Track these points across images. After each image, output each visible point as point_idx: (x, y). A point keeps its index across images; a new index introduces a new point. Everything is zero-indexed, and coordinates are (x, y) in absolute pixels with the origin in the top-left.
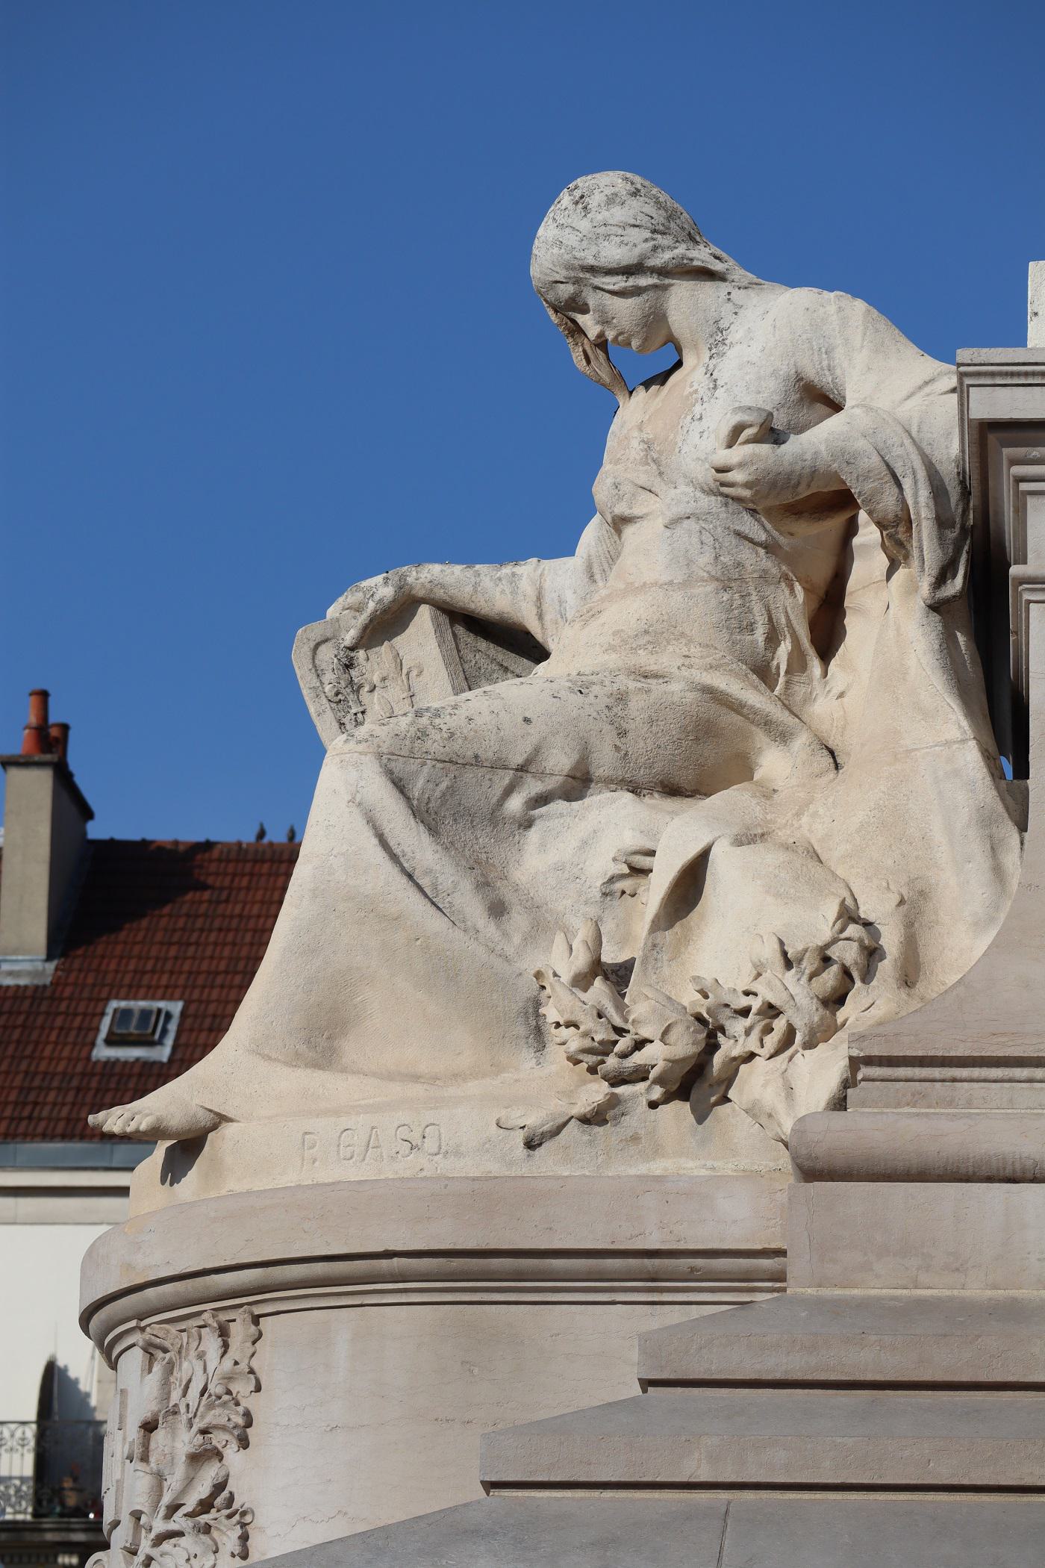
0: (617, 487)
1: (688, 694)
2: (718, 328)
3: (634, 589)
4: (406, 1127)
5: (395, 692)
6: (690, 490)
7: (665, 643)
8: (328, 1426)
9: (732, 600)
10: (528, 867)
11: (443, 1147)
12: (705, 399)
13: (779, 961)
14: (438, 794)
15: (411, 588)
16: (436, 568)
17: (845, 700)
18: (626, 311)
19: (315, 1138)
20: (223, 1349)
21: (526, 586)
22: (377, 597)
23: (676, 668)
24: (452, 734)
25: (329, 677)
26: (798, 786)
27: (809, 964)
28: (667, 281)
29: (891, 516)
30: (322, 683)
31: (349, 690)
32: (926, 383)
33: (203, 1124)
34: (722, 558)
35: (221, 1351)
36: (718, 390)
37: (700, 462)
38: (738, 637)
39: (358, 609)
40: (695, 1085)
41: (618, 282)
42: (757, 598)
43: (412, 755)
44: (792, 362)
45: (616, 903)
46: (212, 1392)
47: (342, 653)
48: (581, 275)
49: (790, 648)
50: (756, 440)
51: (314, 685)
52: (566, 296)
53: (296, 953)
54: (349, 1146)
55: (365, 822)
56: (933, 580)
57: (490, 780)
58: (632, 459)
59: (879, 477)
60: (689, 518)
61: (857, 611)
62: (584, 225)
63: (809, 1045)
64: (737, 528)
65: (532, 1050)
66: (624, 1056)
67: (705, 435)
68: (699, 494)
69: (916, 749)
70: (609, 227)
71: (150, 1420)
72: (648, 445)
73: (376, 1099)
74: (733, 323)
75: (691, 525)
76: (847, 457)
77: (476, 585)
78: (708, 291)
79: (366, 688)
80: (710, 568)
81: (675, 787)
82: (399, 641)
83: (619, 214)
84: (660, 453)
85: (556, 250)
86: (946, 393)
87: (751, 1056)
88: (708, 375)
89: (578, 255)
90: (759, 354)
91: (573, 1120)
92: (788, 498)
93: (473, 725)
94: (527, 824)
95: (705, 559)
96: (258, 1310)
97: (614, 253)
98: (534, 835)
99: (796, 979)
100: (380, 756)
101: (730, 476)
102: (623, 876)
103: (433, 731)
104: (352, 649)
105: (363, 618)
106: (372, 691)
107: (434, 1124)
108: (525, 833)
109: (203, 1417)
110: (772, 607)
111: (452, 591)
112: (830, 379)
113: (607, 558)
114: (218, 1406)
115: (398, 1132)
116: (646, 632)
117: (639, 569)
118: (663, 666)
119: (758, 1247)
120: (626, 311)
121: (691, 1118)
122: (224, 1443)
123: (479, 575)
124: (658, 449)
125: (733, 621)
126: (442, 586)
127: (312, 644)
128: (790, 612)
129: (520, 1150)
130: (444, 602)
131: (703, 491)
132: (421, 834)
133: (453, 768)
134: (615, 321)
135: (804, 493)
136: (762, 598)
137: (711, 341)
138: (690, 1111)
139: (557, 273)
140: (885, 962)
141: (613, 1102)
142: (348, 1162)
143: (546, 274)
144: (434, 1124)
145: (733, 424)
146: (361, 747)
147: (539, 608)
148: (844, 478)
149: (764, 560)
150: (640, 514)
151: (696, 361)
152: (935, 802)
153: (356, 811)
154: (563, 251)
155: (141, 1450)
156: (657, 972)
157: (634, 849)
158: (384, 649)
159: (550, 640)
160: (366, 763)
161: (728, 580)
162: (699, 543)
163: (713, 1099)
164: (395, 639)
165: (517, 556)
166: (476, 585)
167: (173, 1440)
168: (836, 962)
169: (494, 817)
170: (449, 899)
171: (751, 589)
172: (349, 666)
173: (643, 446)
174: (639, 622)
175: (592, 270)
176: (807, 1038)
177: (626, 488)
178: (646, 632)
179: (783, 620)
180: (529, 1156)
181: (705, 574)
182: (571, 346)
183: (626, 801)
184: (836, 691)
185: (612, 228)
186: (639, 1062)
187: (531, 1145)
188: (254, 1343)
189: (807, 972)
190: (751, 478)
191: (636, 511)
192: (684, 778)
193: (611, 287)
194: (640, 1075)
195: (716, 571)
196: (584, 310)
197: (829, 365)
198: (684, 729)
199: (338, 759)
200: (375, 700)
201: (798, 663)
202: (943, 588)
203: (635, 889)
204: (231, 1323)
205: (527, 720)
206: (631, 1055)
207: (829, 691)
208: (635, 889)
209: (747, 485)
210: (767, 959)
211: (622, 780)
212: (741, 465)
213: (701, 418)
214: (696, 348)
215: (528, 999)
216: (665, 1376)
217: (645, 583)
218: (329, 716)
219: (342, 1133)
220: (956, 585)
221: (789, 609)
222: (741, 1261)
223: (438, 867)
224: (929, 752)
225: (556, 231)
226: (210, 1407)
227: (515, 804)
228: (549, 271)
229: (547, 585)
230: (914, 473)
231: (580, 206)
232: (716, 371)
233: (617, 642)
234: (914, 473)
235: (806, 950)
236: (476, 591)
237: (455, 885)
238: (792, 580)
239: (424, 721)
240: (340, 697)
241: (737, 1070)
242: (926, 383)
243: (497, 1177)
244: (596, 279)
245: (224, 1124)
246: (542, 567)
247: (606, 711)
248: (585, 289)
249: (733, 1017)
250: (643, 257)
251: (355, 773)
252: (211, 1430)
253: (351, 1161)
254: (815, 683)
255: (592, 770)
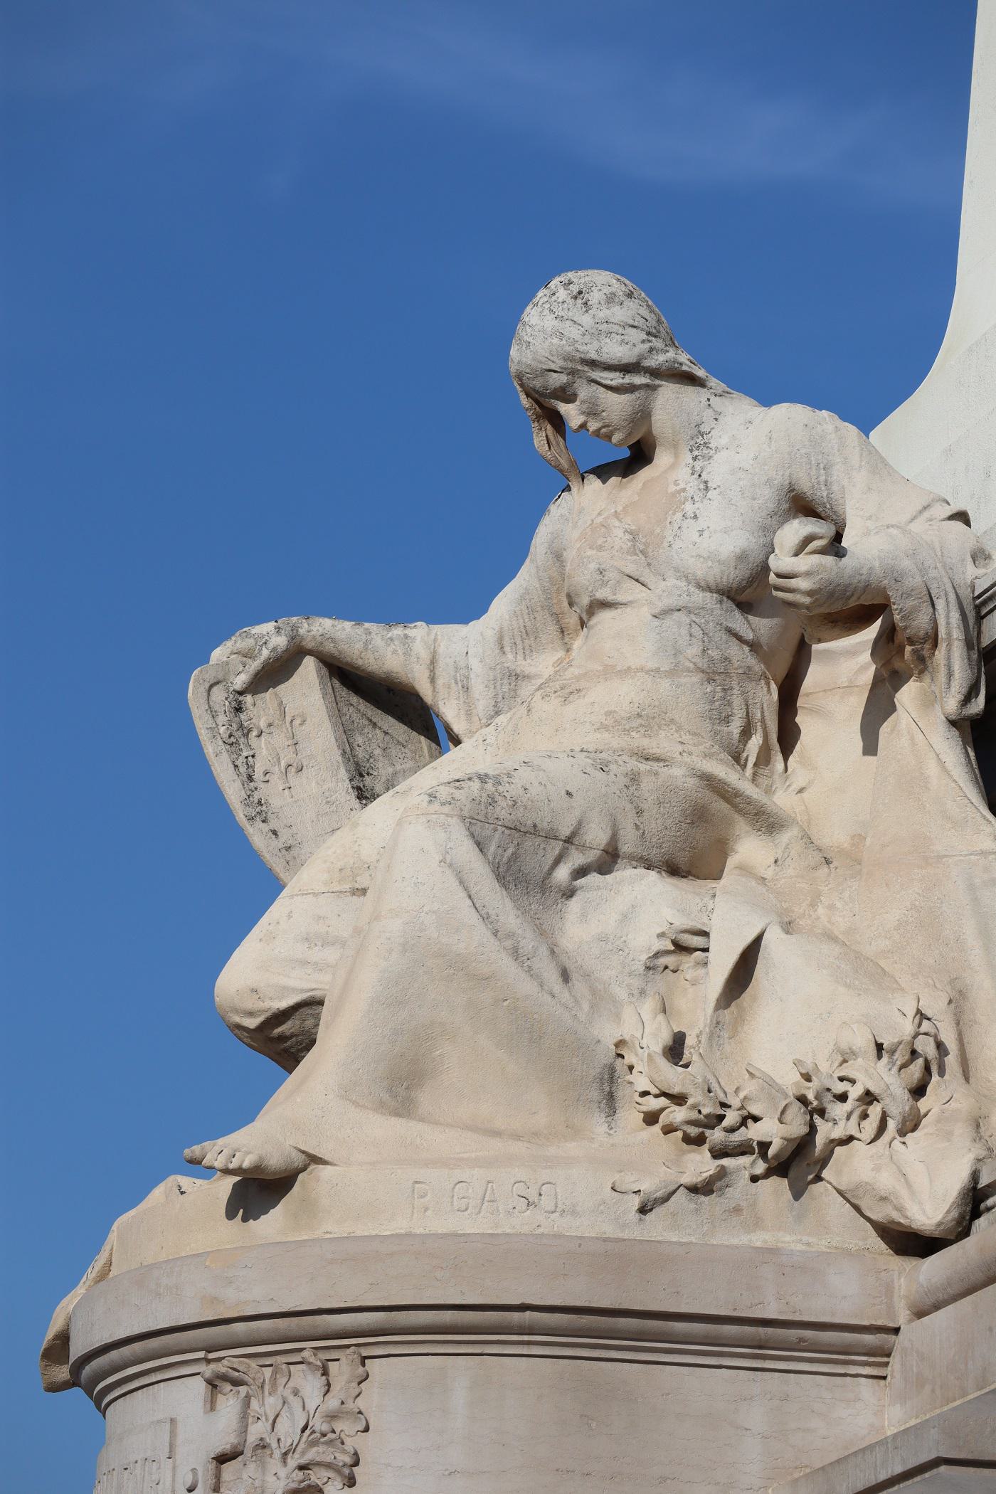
0: (601, 573)
1: (689, 780)
2: (699, 432)
3: (610, 672)
4: (522, 1184)
5: (279, 739)
6: (683, 584)
7: (656, 727)
8: (446, 1470)
9: (714, 692)
10: (571, 936)
11: (559, 1206)
12: (696, 498)
13: (872, 1050)
14: (505, 859)
15: (302, 639)
16: (327, 623)
17: (805, 795)
18: (617, 406)
19: (427, 1188)
20: (327, 1387)
21: (419, 649)
22: (271, 645)
23: (678, 753)
24: (515, 803)
25: (222, 719)
26: (796, 877)
27: (900, 1057)
28: (657, 382)
29: (922, 633)
30: (217, 725)
31: (240, 733)
32: (925, 508)
33: (296, 1165)
34: (710, 652)
35: (324, 1390)
36: (710, 492)
37: (702, 559)
38: (719, 728)
39: (248, 655)
40: (793, 1163)
41: (615, 379)
42: (739, 692)
43: (487, 821)
44: (787, 474)
45: (658, 977)
46: (317, 1428)
47: (231, 696)
48: (579, 367)
49: (761, 742)
50: (822, 551)
51: (211, 726)
52: (558, 385)
53: (384, 1004)
54: (463, 1198)
55: (458, 883)
56: (963, 697)
57: (544, 849)
58: (617, 547)
59: (919, 596)
60: (680, 610)
61: (814, 711)
62: (586, 320)
63: (902, 1133)
64: (730, 625)
65: (603, 1115)
66: (731, 1130)
67: (706, 534)
68: (692, 589)
69: (946, 856)
70: (611, 325)
71: (228, 1452)
72: (634, 535)
73: (477, 1154)
74: (713, 428)
75: (683, 617)
76: (895, 575)
77: (367, 643)
78: (690, 394)
79: (255, 733)
80: (697, 660)
81: (675, 867)
82: (282, 688)
83: (619, 314)
84: (647, 545)
85: (556, 341)
86: (944, 520)
87: (851, 1139)
88: (696, 476)
89: (581, 348)
90: (751, 462)
91: (682, 1188)
92: (837, 607)
93: (528, 795)
94: (569, 893)
95: (693, 651)
96: (366, 1352)
97: (616, 351)
98: (574, 904)
99: (887, 1069)
100: (463, 819)
101: (793, 583)
102: (668, 952)
103: (500, 797)
104: (240, 693)
105: (255, 665)
106: (259, 736)
107: (550, 1183)
108: (566, 902)
109: (303, 1453)
110: (751, 702)
111: (342, 647)
112: (825, 494)
113: (521, 632)
114: (323, 1443)
115: (457, 1186)
116: (639, 715)
117: (622, 653)
118: (666, 750)
119: (866, 1323)
120: (617, 406)
121: (789, 1195)
122: (325, 1480)
123: (370, 633)
124: (644, 540)
125: (714, 712)
126: (333, 640)
127: (207, 686)
128: (765, 708)
129: (633, 1215)
130: (332, 656)
131: (699, 586)
132: (505, 898)
133: (517, 835)
134: (604, 414)
135: (853, 603)
136: (743, 693)
137: (692, 443)
138: (788, 1188)
139: (553, 362)
140: (949, 1056)
141: (722, 1173)
142: (462, 1213)
143: (540, 362)
144: (550, 1183)
145: (805, 534)
146: (447, 809)
147: (431, 671)
148: (891, 594)
149: (749, 658)
150: (624, 601)
151: (672, 460)
152: (968, 907)
153: (449, 872)
154: (564, 342)
155: (214, 1481)
156: (720, 1049)
157: (685, 927)
158: (269, 695)
159: (441, 703)
160: (454, 826)
161: (713, 673)
162: (688, 635)
163: (810, 1177)
164: (279, 687)
165: (406, 618)
166: (367, 643)
167: (264, 1474)
168: (920, 1055)
169: (544, 885)
170: (528, 963)
171: (734, 684)
172: (238, 709)
173: (628, 536)
174: (631, 705)
175: (593, 364)
176: (900, 1126)
177: (612, 575)
178: (639, 715)
179: (759, 715)
180: (640, 1220)
181: (691, 665)
182: (535, 430)
183: (653, 878)
184: (796, 786)
185: (613, 326)
186: (823, 1142)
187: (643, 1210)
188: (360, 1383)
189: (899, 1063)
190: (815, 587)
191: (620, 598)
192: (682, 859)
193: (608, 382)
194: (743, 1149)
195: (702, 663)
196: (570, 399)
197: (826, 481)
198: (684, 811)
199: (424, 819)
200: (263, 746)
201: (764, 759)
202: (968, 706)
203: (678, 966)
204: (329, 1363)
205: (569, 794)
206: (738, 1130)
207: (789, 786)
208: (678, 966)
209: (810, 593)
210: (860, 1048)
211: (640, 858)
212: (808, 574)
213: (695, 517)
214: (675, 448)
215: (605, 1066)
216: (962, 1456)
217: (629, 668)
218: (225, 758)
219: (456, 1184)
220: (979, 704)
221: (765, 705)
222: (846, 1335)
223: (520, 931)
224: (962, 860)
225: (555, 323)
226: (313, 1443)
227: (562, 874)
228: (544, 359)
229: (442, 649)
230: (946, 595)
231: (580, 301)
232: (704, 472)
233: (610, 722)
234: (946, 595)
235: (900, 1043)
236: (366, 649)
237: (535, 949)
238: (769, 678)
239: (490, 787)
240: (232, 739)
241: (832, 1152)
242: (925, 508)
243: (624, 1240)
244: (594, 373)
245: (312, 1167)
246: (434, 632)
247: (625, 790)
248: (578, 381)
249: (834, 1101)
250: (641, 357)
251: (443, 834)
252: (310, 1467)
253: (466, 1213)
254: (776, 777)
255: (620, 846)
